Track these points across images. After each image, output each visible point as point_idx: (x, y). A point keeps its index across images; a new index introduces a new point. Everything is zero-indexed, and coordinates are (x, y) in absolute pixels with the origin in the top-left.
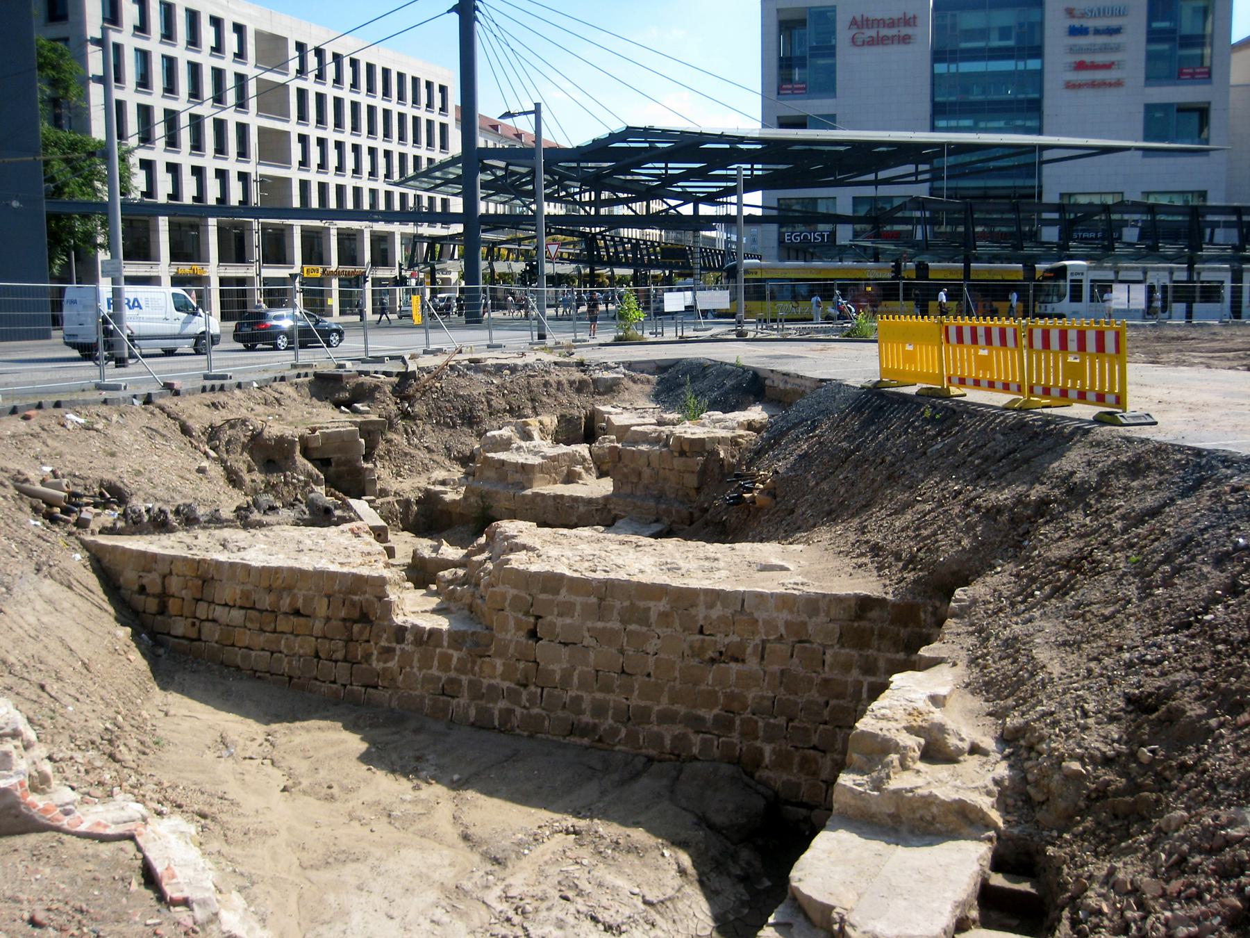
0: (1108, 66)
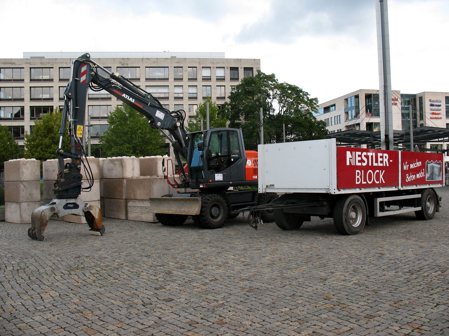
0: (438, 114)
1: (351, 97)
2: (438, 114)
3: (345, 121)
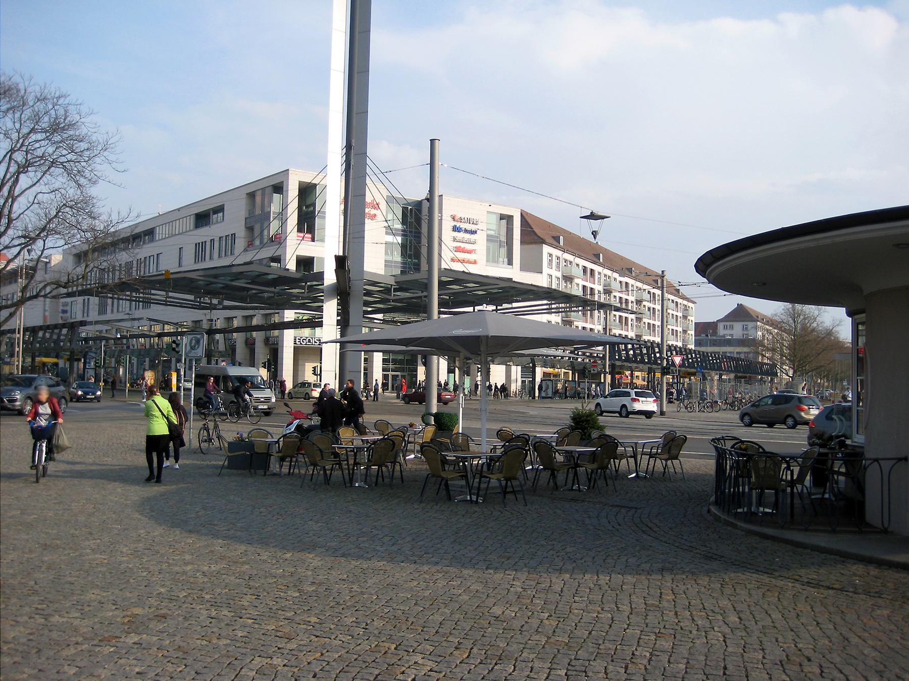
0: (469, 252)
1: (263, 189)
2: (469, 252)
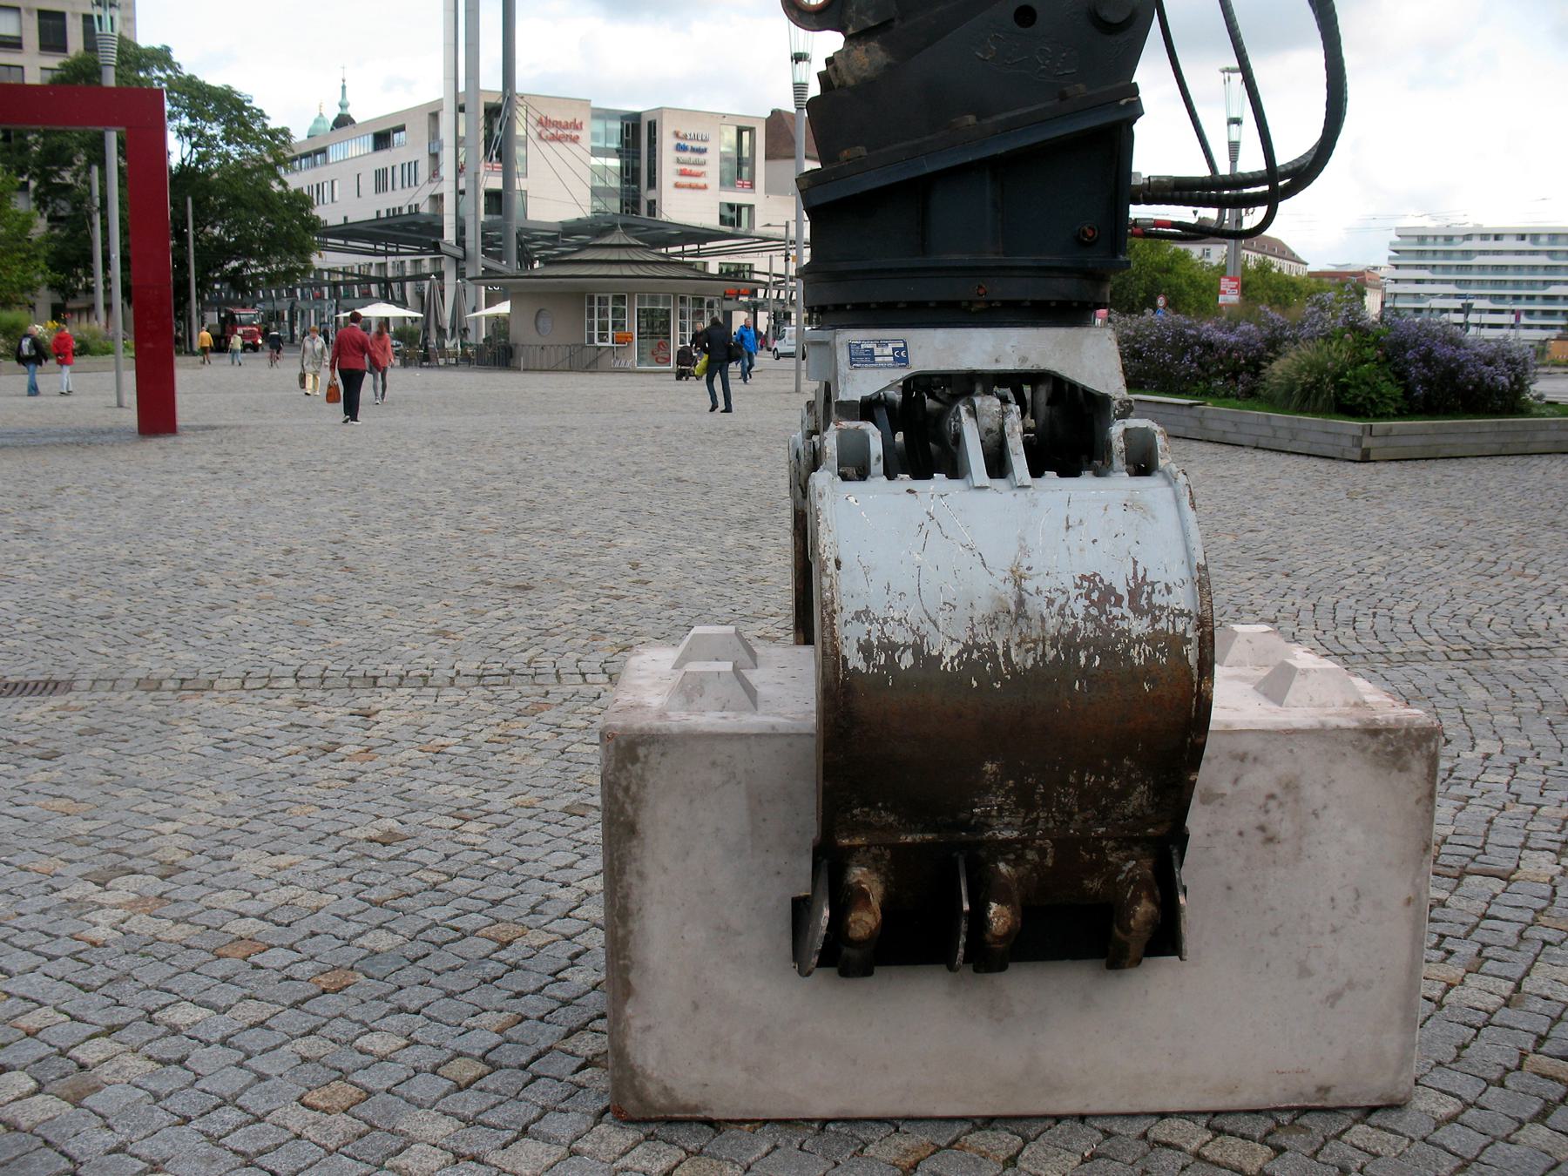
0: (698, 175)
3: (430, 181)
